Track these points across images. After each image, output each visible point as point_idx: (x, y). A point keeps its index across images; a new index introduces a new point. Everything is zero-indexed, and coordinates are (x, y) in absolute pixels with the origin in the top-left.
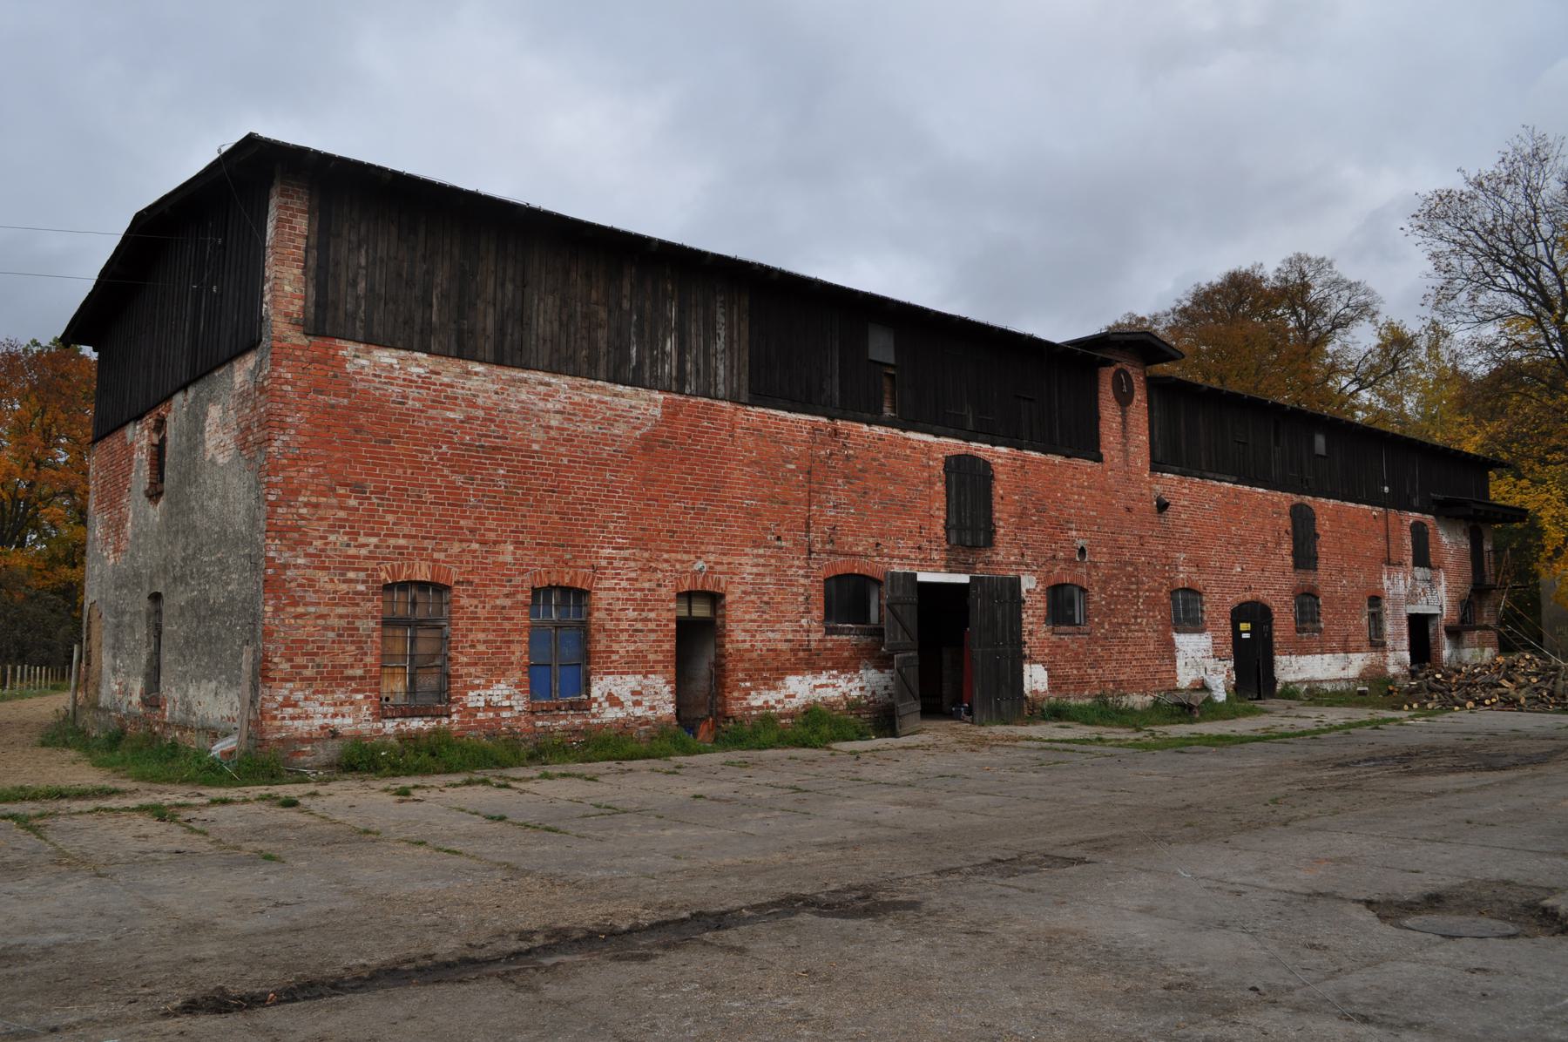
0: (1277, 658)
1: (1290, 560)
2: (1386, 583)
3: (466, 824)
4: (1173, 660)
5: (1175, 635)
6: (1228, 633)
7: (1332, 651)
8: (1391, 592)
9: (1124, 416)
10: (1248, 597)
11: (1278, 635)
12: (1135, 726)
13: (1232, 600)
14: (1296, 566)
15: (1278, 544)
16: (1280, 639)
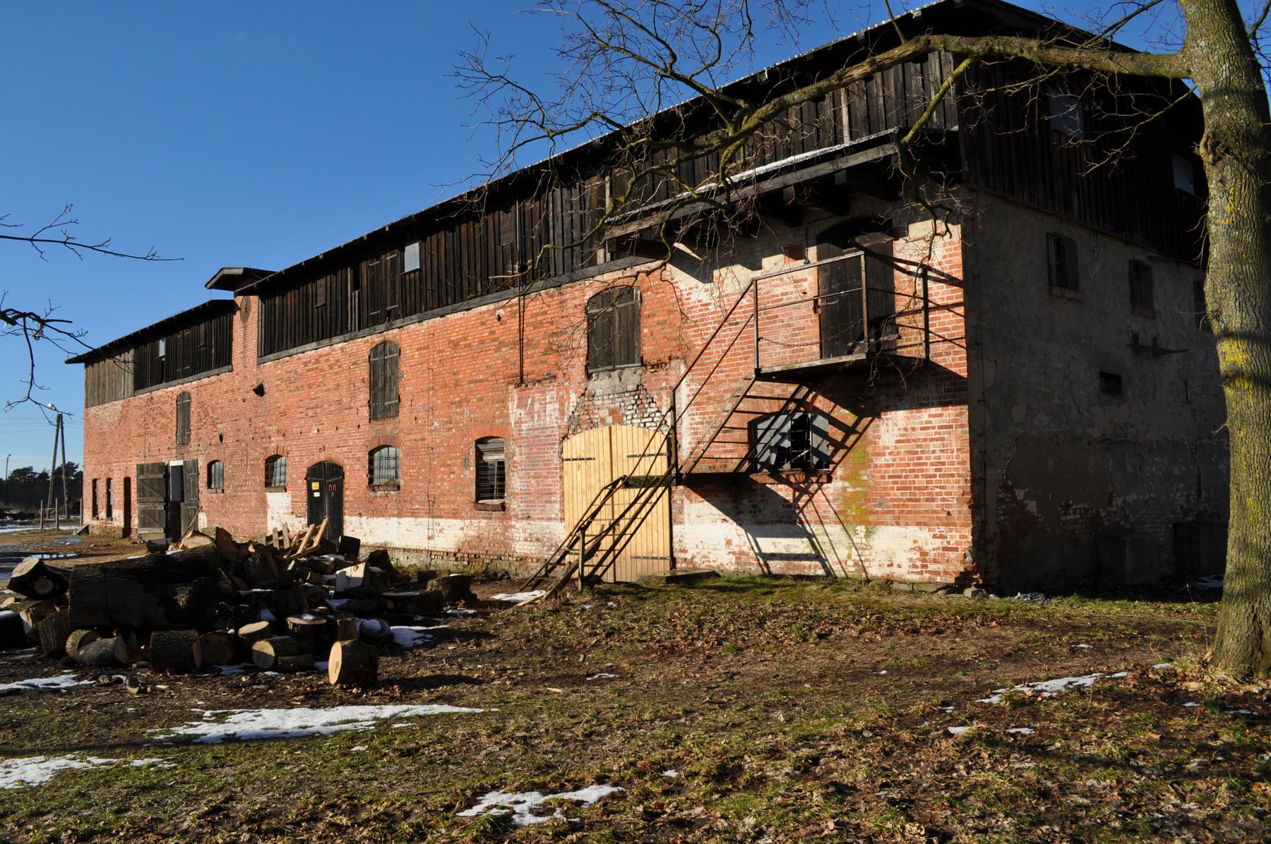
0: (346, 518)
1: (365, 412)
2: (514, 412)
3: (36, 538)
4: (265, 513)
5: (965, 374)
6: (304, 492)
7: (414, 514)
8: (524, 427)
9: (245, 327)
10: (322, 457)
11: (348, 495)
12: (606, 595)
13: (309, 461)
14: (373, 417)
15: (353, 397)
16: (351, 499)
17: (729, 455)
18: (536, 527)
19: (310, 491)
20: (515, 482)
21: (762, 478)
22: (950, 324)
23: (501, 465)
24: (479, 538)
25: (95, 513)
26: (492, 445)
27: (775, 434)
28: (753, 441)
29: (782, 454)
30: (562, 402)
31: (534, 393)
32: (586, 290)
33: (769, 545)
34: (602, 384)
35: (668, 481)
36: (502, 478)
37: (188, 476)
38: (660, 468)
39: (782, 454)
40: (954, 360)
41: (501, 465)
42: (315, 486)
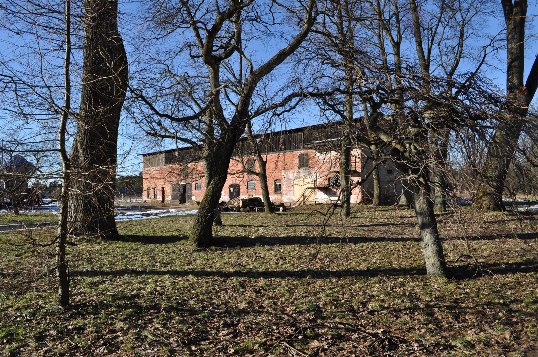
13: (232, 183)
17: (326, 184)
18: (288, 197)
19: (230, 190)
20: (283, 188)
21: (331, 187)
22: (359, 165)
23: (280, 185)
24: (275, 199)
25: (148, 196)
26: (278, 181)
27: (333, 180)
28: (329, 181)
29: (334, 184)
30: (294, 173)
31: (287, 172)
32: (299, 152)
33: (332, 198)
34: (301, 170)
35: (315, 188)
36: (280, 188)
37: (187, 187)
38: (313, 186)
39: (334, 184)
40: (359, 170)
41: (280, 185)
42: (231, 189)
